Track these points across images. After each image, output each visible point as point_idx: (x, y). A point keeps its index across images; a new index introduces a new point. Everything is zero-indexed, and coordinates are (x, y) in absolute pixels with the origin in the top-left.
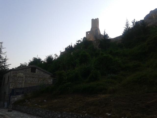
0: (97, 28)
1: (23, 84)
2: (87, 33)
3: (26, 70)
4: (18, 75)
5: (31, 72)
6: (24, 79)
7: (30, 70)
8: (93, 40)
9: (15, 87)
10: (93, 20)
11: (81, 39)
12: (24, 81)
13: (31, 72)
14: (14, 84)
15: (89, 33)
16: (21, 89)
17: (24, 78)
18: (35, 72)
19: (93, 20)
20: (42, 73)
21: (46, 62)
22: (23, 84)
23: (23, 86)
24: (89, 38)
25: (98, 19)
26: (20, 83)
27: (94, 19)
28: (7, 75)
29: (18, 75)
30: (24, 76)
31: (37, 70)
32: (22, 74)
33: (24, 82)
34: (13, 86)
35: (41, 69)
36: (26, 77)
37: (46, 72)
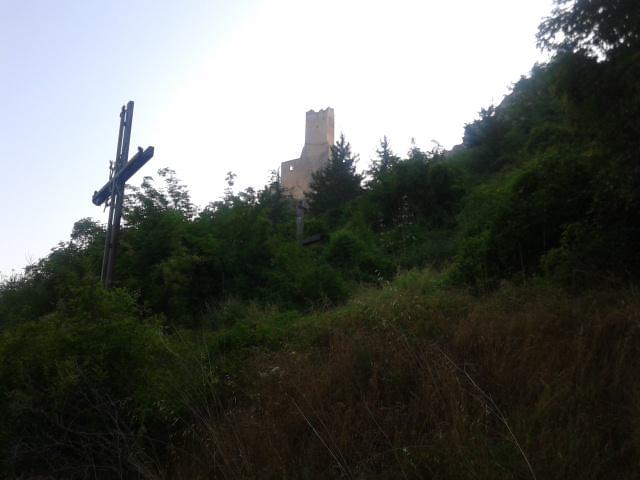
10: (310, 114)
15: (291, 168)
19: (310, 114)
24: (293, 188)
25: (332, 110)
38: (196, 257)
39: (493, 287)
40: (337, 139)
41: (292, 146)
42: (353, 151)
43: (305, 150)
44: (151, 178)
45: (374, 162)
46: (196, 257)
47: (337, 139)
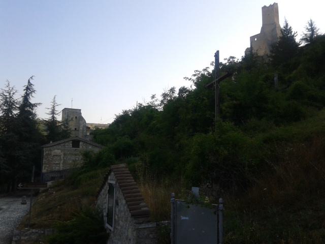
0: (276, 25)
1: (61, 165)
2: (252, 38)
3: (64, 146)
4: (53, 153)
5: (73, 147)
6: (62, 158)
7: (71, 144)
8: (266, 52)
9: (49, 170)
10: (264, 8)
11: (225, 59)
12: (63, 160)
13: (73, 147)
14: (47, 166)
15: (256, 39)
16: (59, 172)
17: (62, 156)
18: (79, 147)
19: (264, 8)
20: (90, 147)
21: (160, 109)
22: (61, 165)
23: (61, 168)
24: (257, 50)
25: (277, 4)
26: (57, 164)
27: (268, 5)
28: (255, 49)
29: (53, 153)
30: (62, 154)
31: (81, 143)
32: (59, 151)
33: (62, 162)
34: (46, 168)
35: (60, 142)
36: (65, 154)
37: (96, 146)
38: (235, 102)
39: (221, 118)
40: (282, 25)
41: (256, 28)
42: (294, 31)
43: (262, 28)
44: (208, 68)
45: (306, 35)
46: (235, 102)
47: (282, 25)
